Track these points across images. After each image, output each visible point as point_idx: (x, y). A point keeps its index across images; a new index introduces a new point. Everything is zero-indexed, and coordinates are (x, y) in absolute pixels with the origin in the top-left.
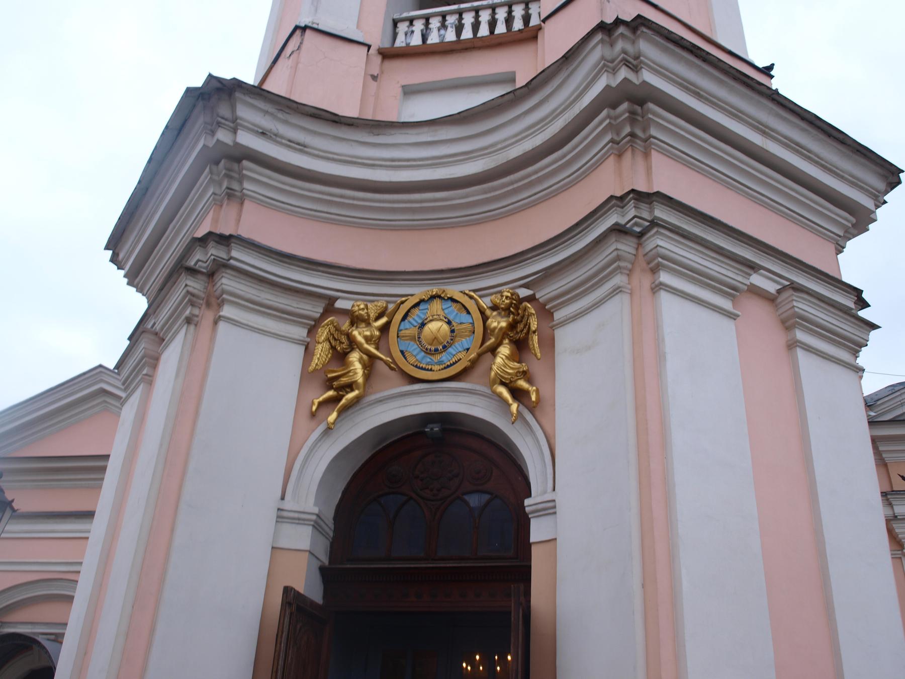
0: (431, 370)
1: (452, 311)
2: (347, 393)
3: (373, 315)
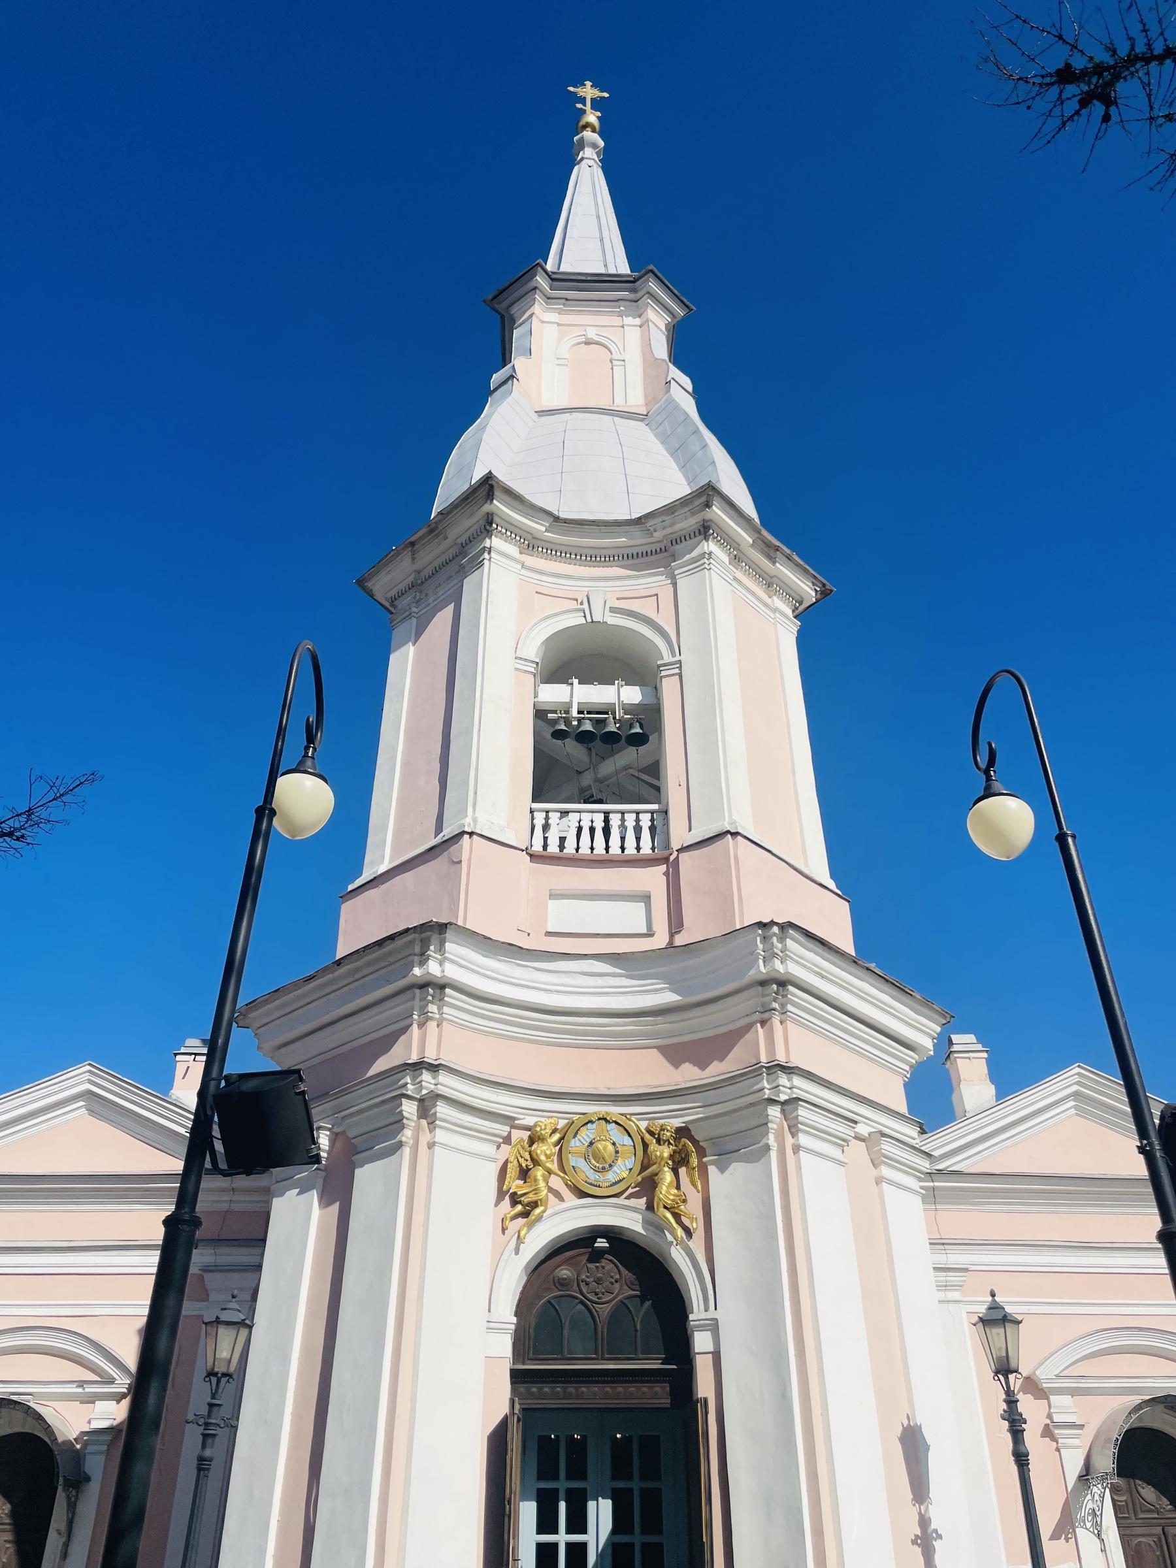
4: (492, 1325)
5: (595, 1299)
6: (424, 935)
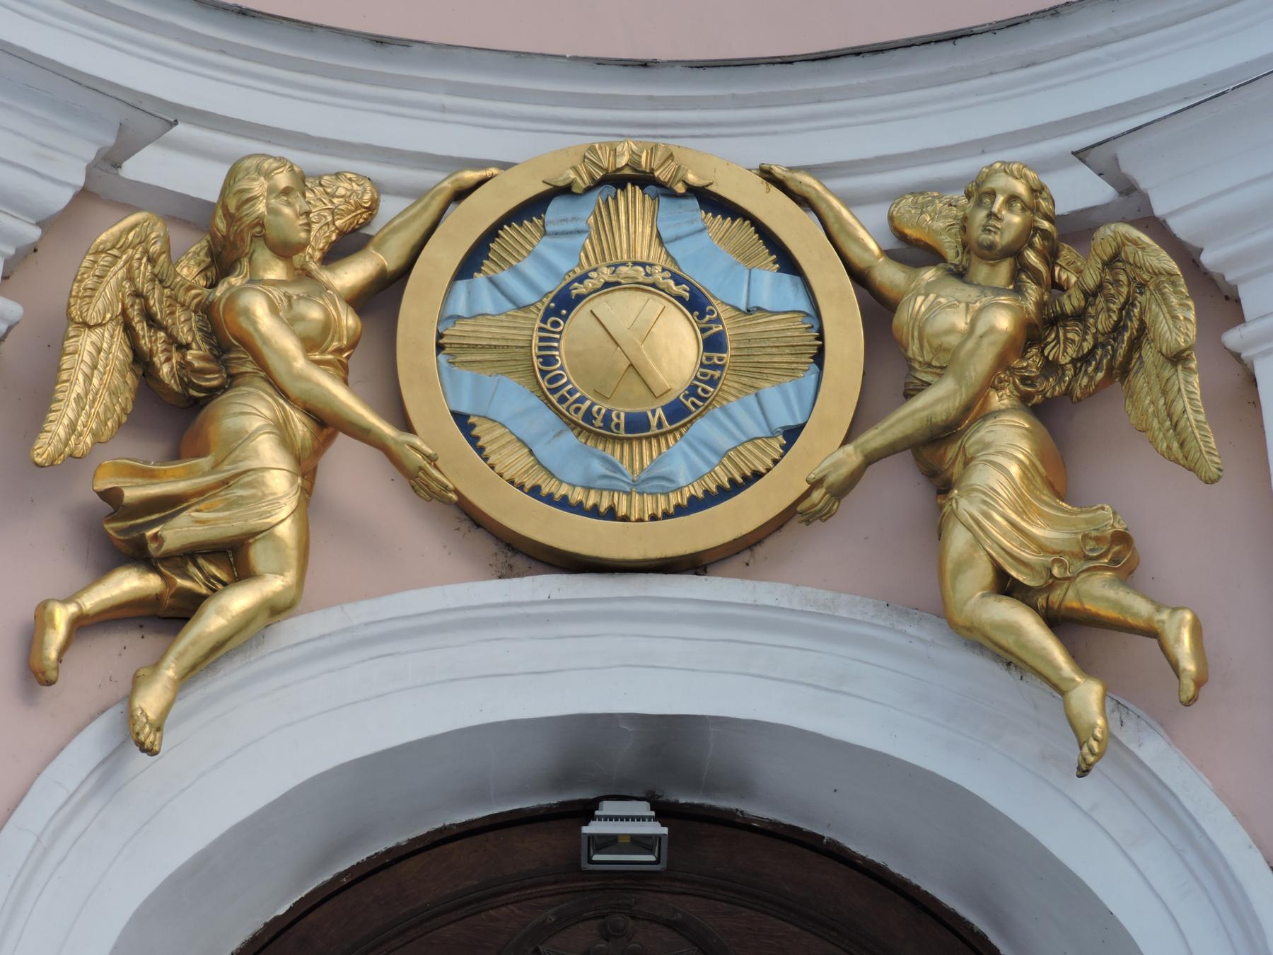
0: (611, 514)
1: (710, 253)
2: (216, 587)
3: (321, 237)
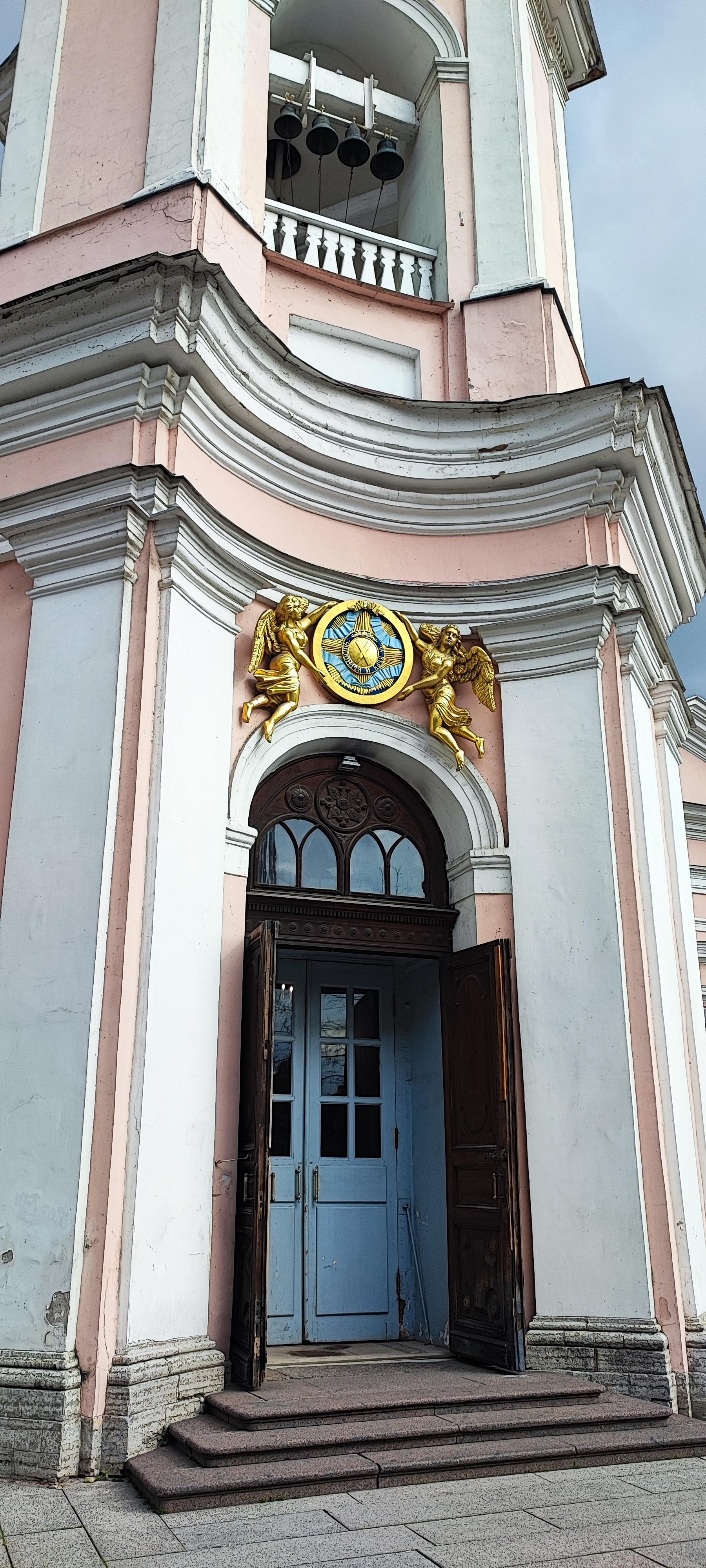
0: (356, 692)
4: (231, 834)
5: (337, 825)
6: (169, 281)
